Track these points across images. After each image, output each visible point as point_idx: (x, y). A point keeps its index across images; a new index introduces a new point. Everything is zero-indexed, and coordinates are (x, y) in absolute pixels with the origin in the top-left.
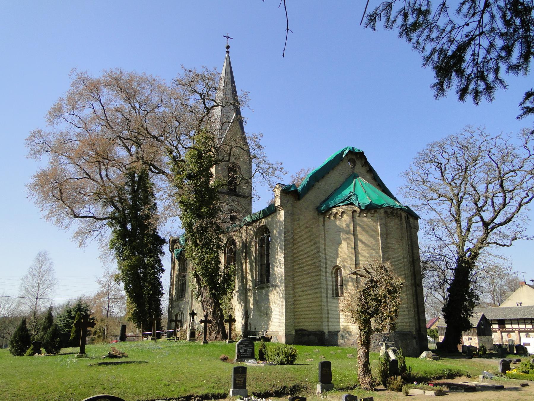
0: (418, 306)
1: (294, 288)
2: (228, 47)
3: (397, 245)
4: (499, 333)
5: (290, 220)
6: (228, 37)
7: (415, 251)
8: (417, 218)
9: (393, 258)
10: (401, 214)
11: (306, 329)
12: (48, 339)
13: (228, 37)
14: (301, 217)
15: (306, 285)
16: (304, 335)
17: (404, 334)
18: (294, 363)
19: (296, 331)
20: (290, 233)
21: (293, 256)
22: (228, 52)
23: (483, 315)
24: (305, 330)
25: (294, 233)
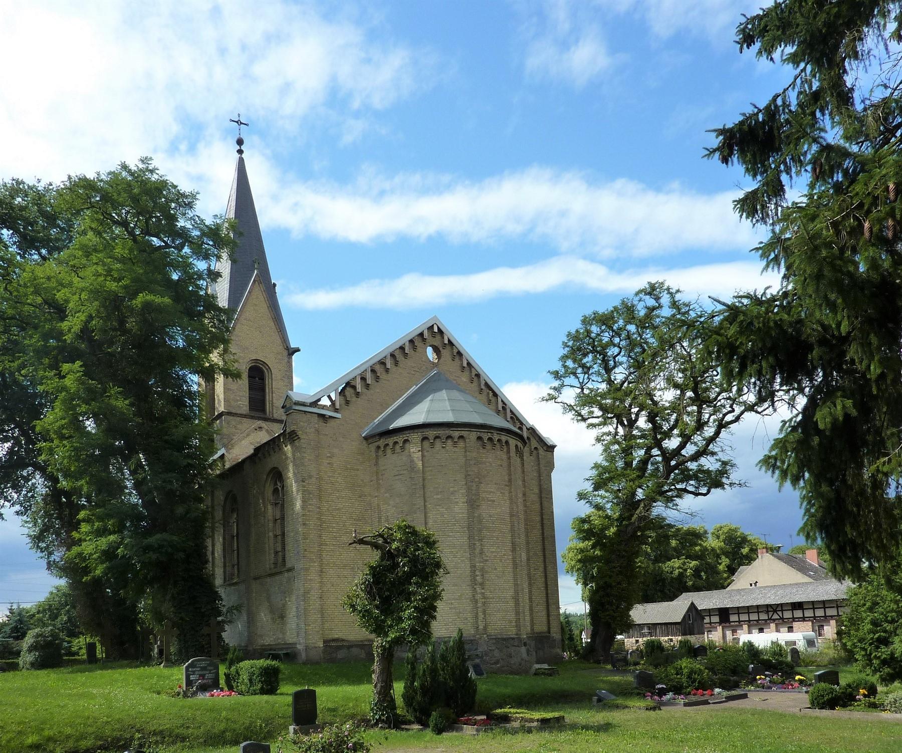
0: (547, 594)
1: (321, 571)
2: (240, 142)
3: (499, 494)
4: (720, 629)
5: (611, 483)
6: (239, 123)
7: (545, 504)
8: (551, 448)
9: (490, 516)
10: (507, 442)
11: (344, 637)
12: (684, 660)
13: (239, 123)
14: (335, 451)
15: (345, 566)
16: (339, 648)
17: (504, 639)
18: (278, 691)
19: (325, 642)
20: (314, 479)
21: (319, 519)
22: (240, 152)
23: (692, 604)
24: (343, 640)
25: (320, 479)
